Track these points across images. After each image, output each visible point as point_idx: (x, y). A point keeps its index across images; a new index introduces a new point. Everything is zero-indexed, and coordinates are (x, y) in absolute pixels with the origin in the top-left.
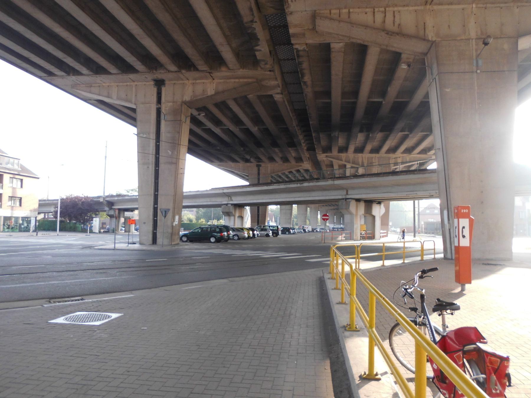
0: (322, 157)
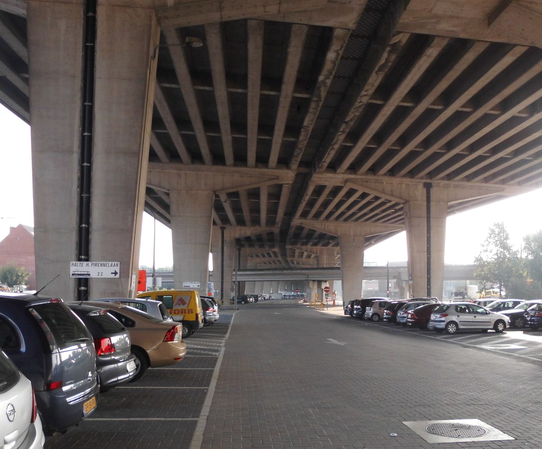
0: (288, 247)
